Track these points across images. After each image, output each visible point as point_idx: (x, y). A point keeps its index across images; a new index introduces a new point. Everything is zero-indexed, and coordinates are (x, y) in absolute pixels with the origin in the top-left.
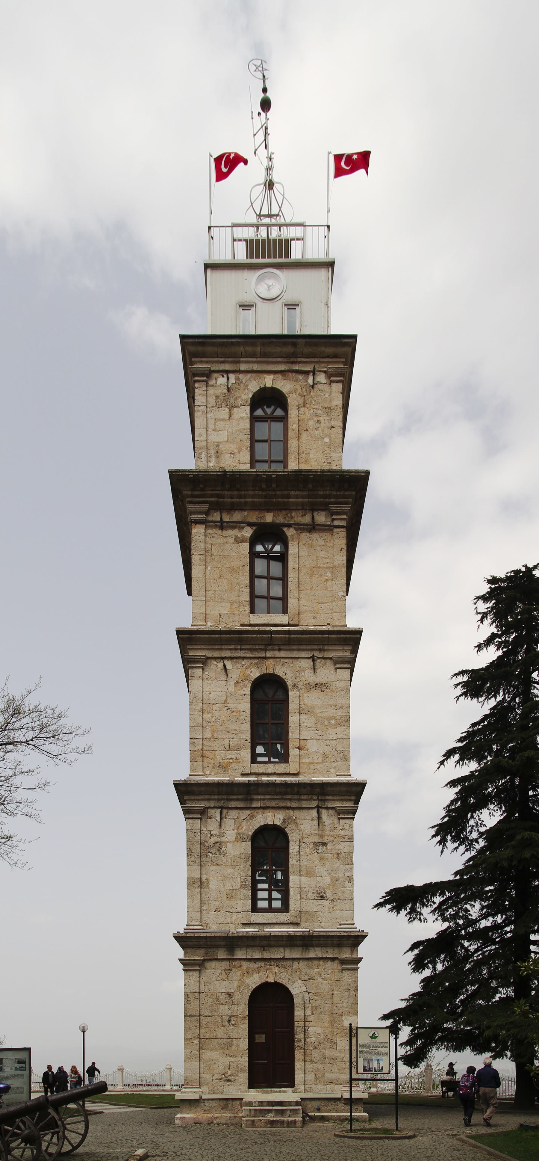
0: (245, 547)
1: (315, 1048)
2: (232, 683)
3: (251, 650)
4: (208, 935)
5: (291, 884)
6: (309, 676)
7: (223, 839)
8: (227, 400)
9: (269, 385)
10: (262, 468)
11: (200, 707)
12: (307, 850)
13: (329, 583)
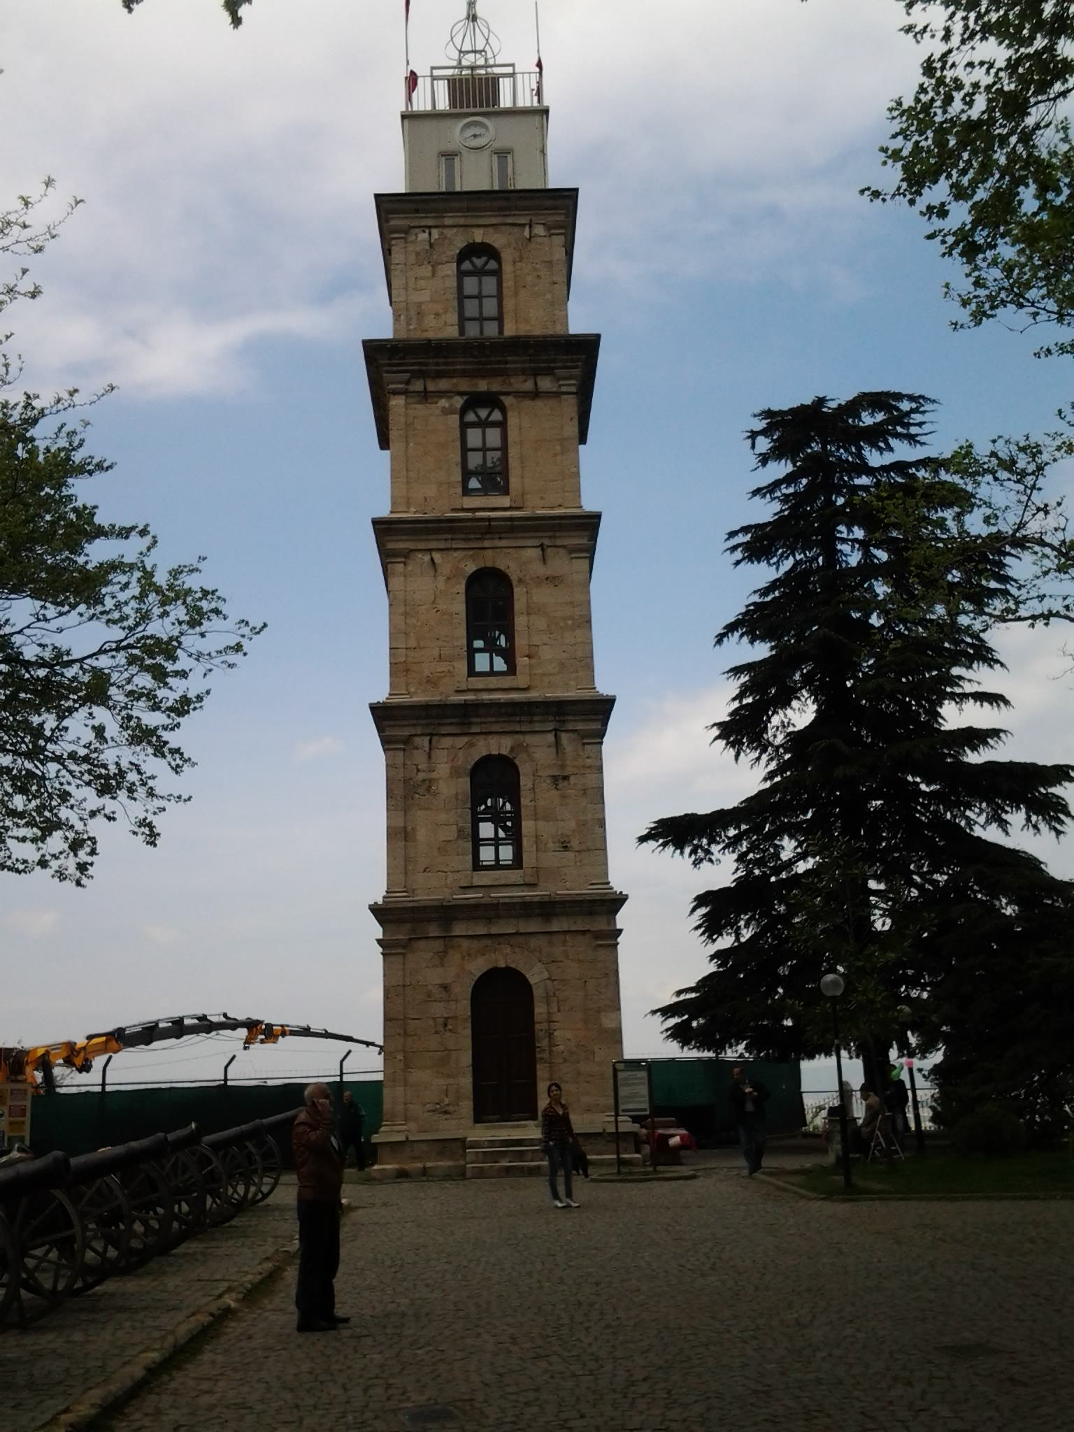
0: (454, 419)
1: (565, 1061)
2: (441, 579)
3: (465, 540)
4: (415, 904)
5: (524, 831)
6: (539, 569)
7: (434, 775)
8: (429, 256)
9: (478, 240)
10: (472, 330)
11: (402, 609)
12: (546, 785)
13: (559, 457)
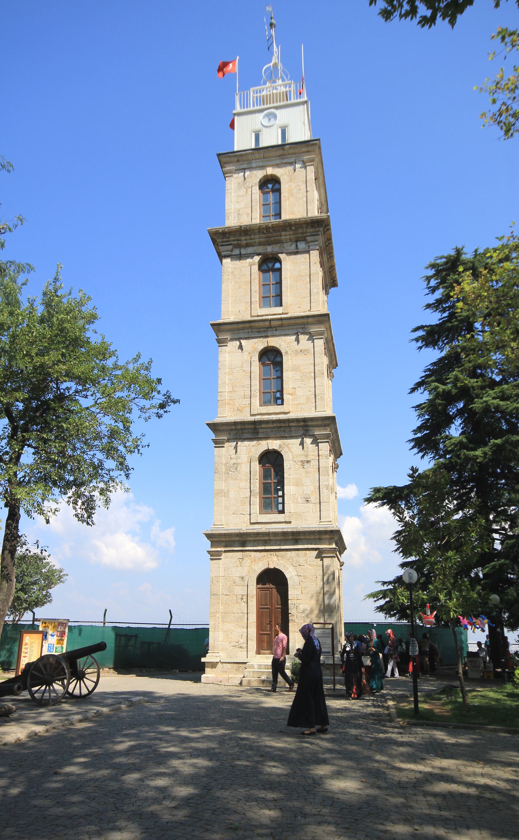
7: (239, 461)
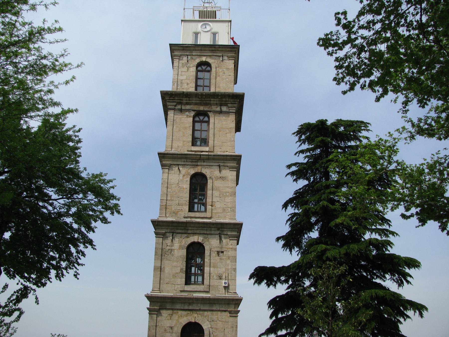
7: (173, 248)
